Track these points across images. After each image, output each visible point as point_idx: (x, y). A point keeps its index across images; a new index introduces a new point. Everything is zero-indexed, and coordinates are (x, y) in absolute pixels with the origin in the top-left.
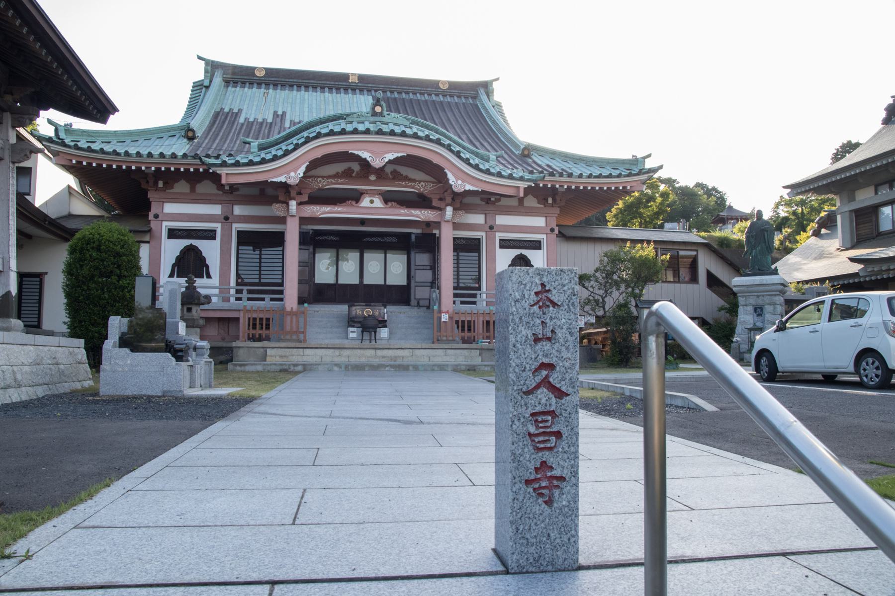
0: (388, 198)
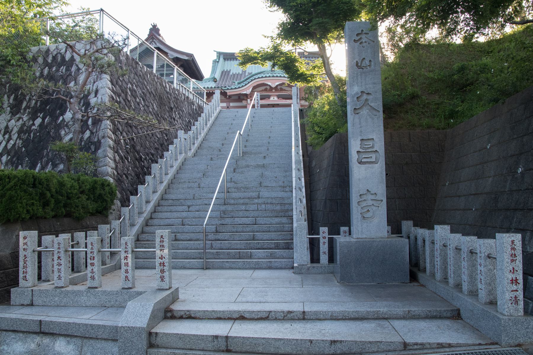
0: (279, 97)
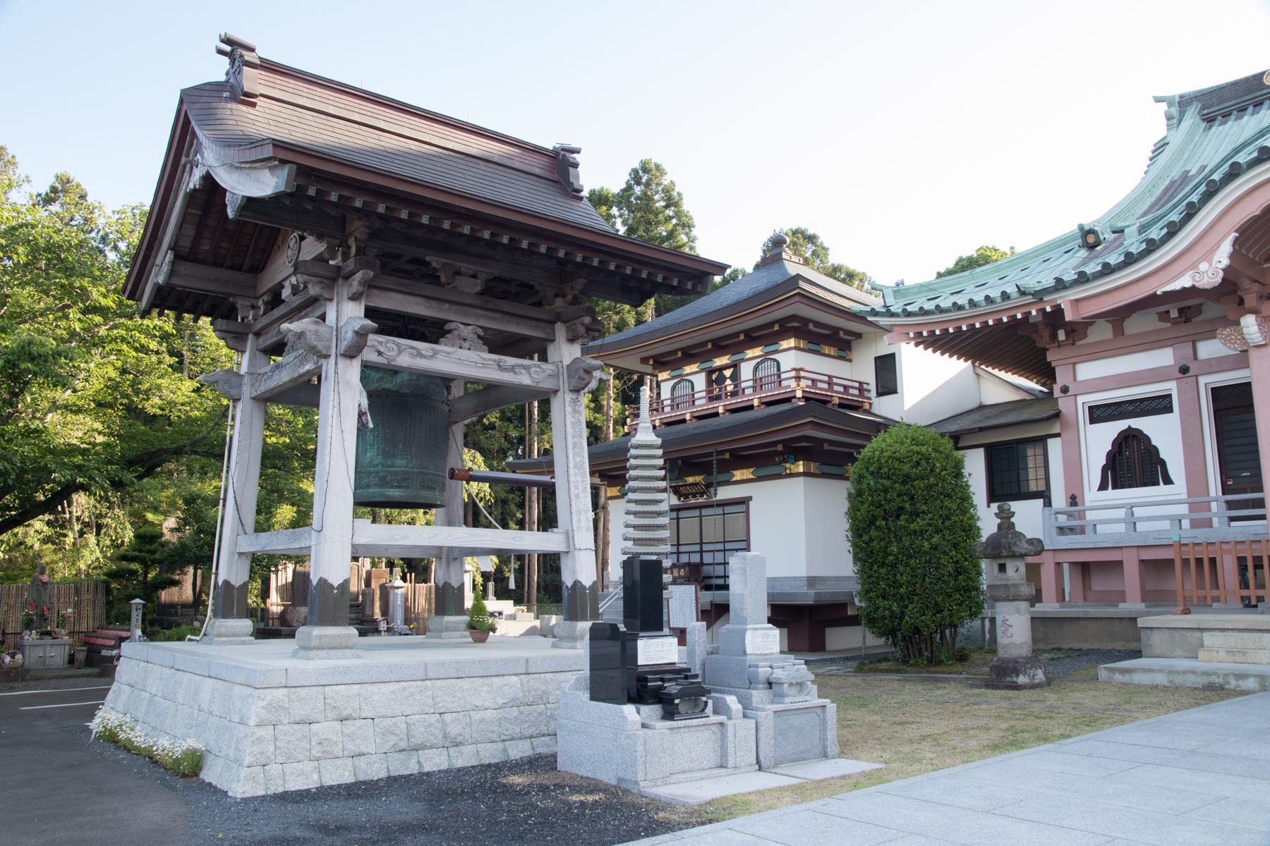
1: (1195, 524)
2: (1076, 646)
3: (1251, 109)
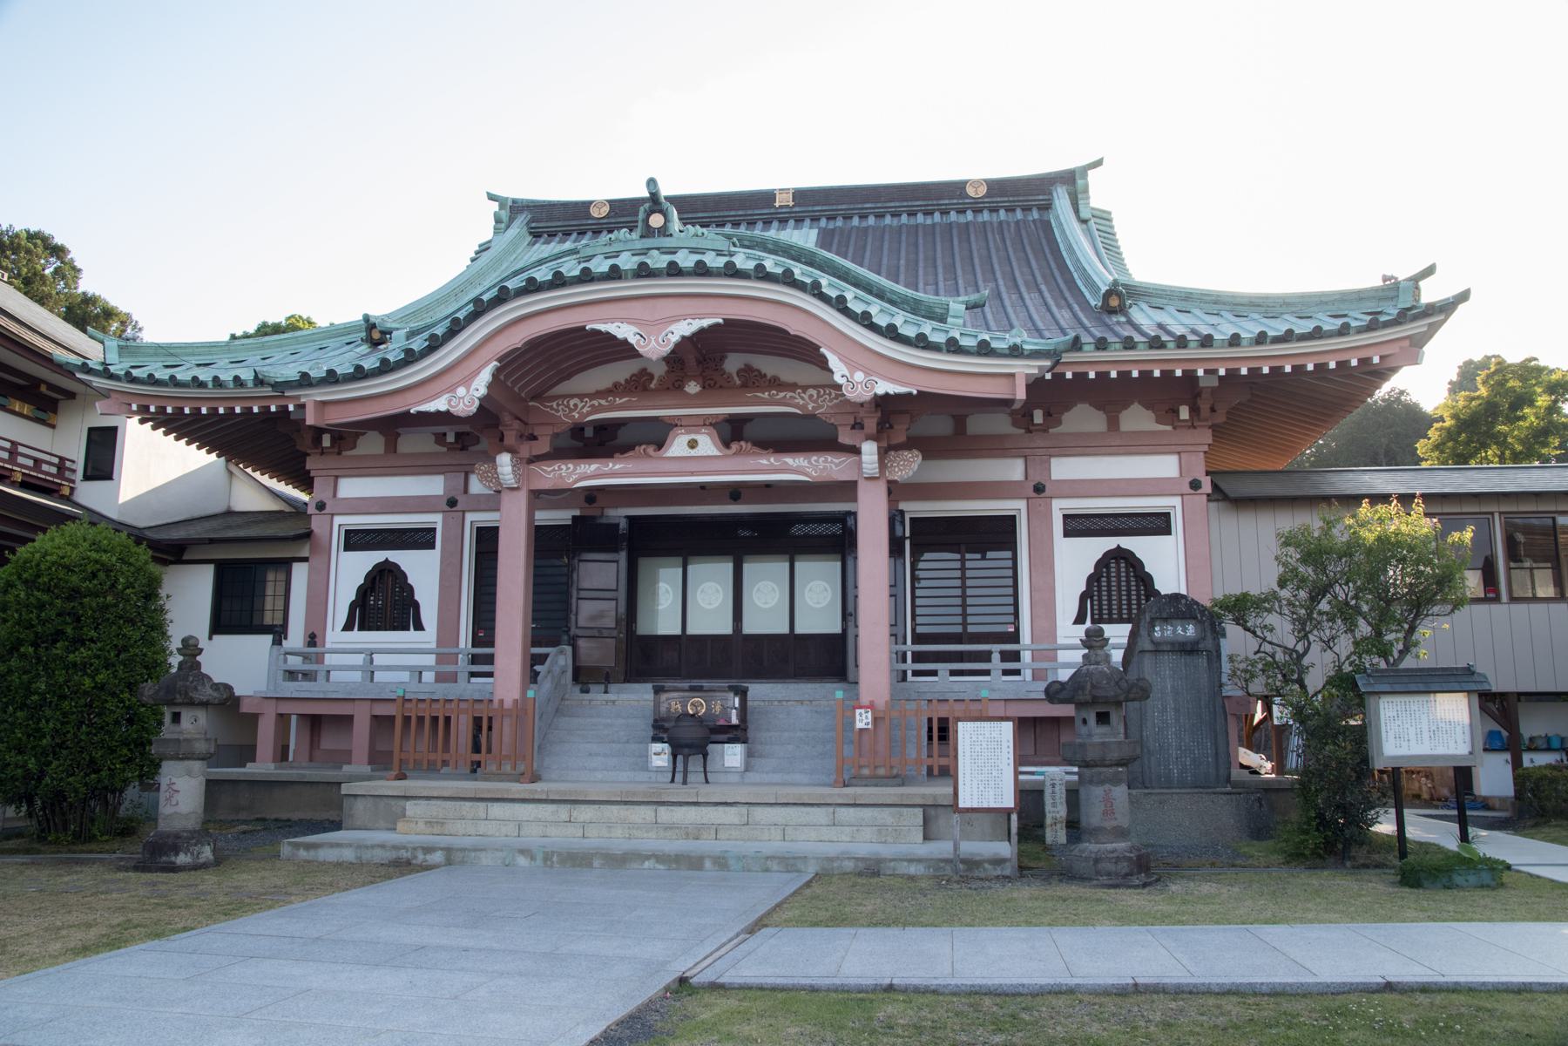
0: (733, 432)
1: (440, 678)
2: (284, 816)
3: (574, 235)
